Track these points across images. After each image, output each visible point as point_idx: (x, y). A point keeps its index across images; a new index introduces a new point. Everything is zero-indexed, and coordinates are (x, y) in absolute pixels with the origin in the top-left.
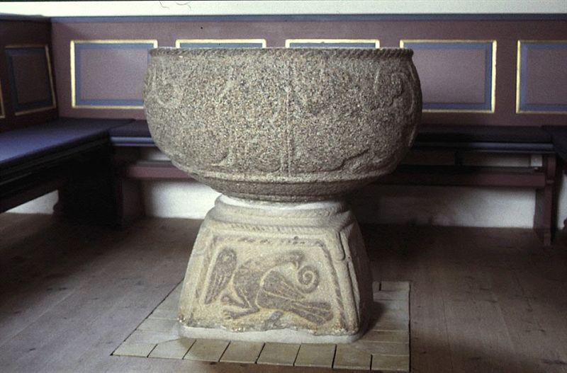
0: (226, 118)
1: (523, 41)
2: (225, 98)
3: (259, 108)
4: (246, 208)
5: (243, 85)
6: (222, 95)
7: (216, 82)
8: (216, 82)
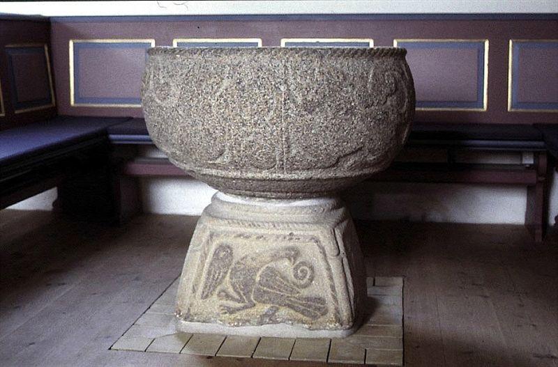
2: (221, 96)
5: (239, 83)
6: (218, 94)
7: (212, 80)
8: (212, 80)
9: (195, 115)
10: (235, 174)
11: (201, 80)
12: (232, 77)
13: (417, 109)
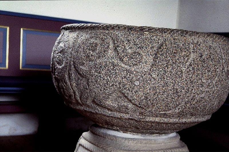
0: (190, 80)
1: (25, 29)
2: (190, 65)
3: (210, 73)
4: (143, 140)
5: (201, 56)
6: (188, 63)
7: (183, 53)
8: (183, 53)
9: (168, 78)
10: (174, 120)
11: (175, 53)
12: (196, 52)
13: (51, 70)
